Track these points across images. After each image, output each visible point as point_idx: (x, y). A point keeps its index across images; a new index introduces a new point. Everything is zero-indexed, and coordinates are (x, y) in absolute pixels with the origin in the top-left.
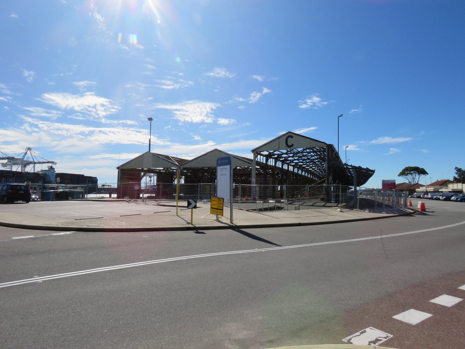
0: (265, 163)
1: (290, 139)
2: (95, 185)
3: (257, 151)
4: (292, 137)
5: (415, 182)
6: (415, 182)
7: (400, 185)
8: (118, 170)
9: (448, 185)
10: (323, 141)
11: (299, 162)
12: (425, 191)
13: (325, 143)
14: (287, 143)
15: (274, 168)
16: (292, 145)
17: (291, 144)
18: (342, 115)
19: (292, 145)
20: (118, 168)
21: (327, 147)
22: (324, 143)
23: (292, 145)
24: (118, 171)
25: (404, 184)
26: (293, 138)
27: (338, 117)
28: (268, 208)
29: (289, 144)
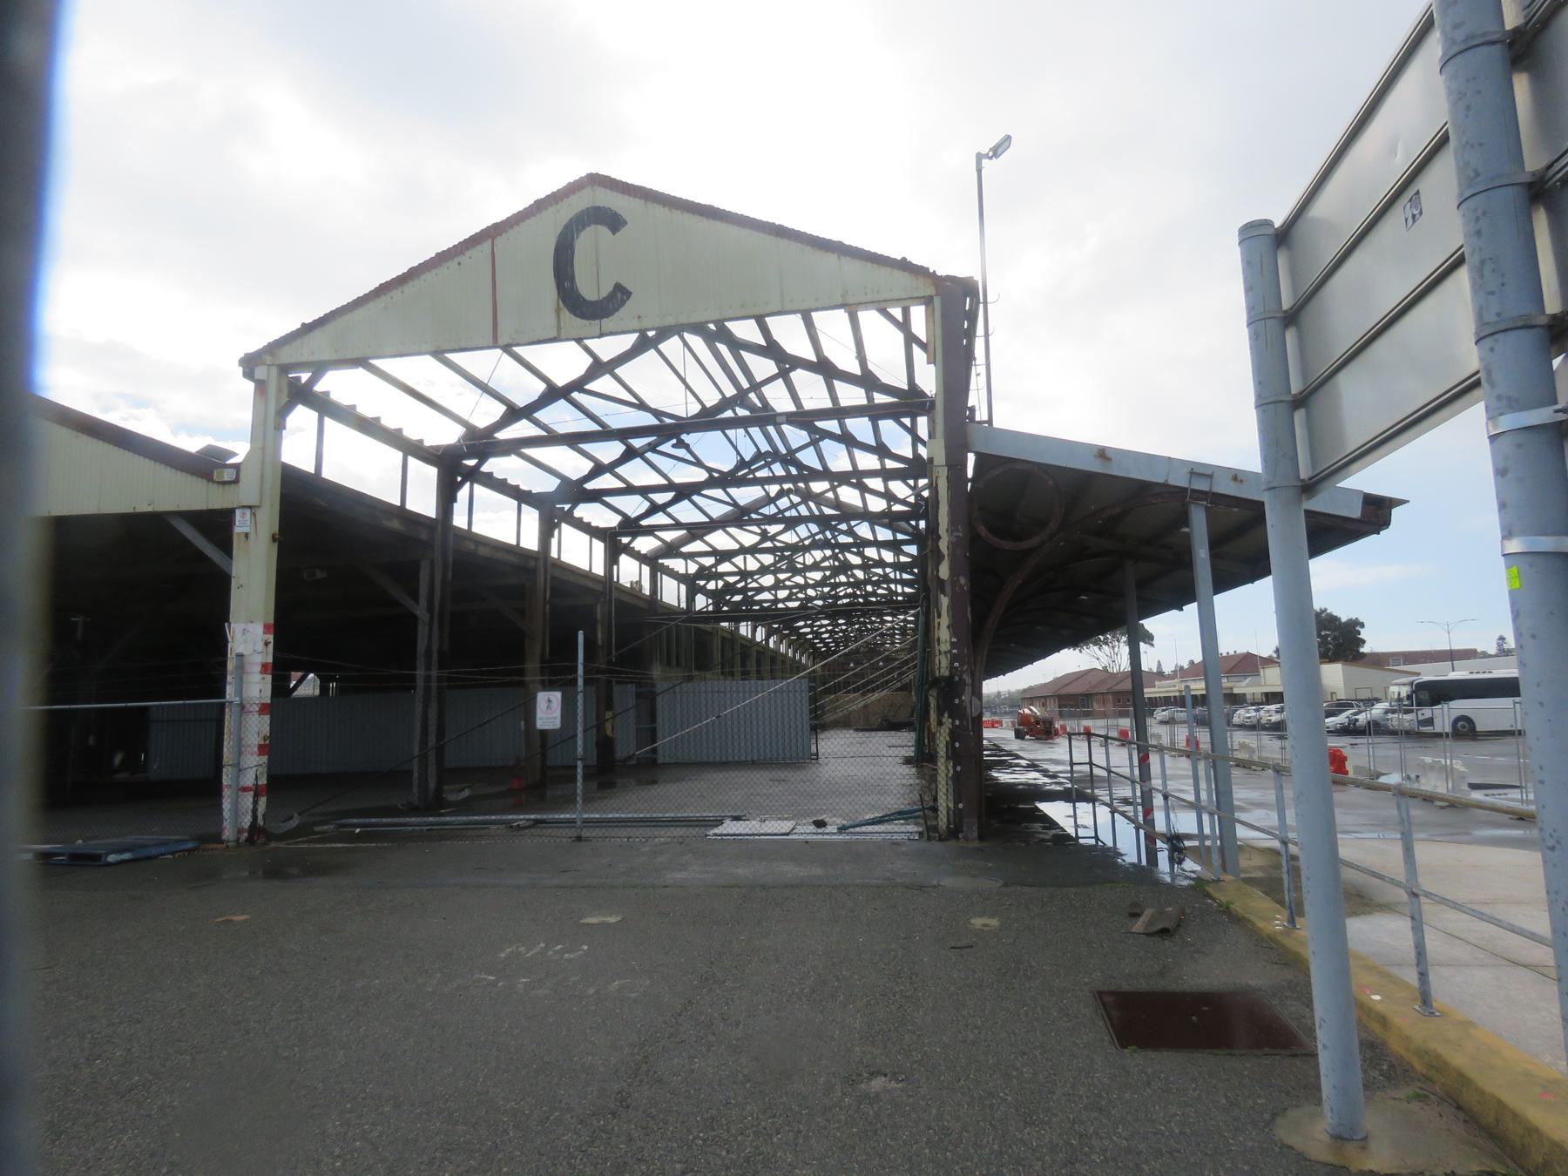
0: (602, 574)
2: (441, 673)
3: (287, 356)
4: (614, 222)
5: (1120, 666)
6: (1120, 666)
7: (1085, 674)
9: (1262, 670)
10: (897, 255)
11: (786, 603)
12: (1175, 697)
13: (920, 272)
14: (572, 279)
15: (776, 652)
16: (612, 295)
17: (606, 290)
21: (937, 301)
22: (904, 265)
25: (1091, 674)
26: (623, 231)
27: (980, 157)
28: (1187, 489)
29: (589, 288)
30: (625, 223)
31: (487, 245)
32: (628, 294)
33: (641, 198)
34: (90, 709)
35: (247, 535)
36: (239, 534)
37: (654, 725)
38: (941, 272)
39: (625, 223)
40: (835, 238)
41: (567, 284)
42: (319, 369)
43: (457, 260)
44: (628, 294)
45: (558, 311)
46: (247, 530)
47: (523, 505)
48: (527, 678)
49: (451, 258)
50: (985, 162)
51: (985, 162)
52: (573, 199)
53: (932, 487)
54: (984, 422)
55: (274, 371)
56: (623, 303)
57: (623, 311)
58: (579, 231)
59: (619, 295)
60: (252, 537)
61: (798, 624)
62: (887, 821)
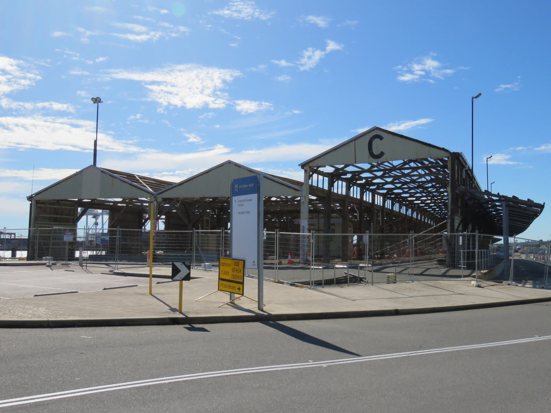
1: (376, 142)
4: (381, 138)
8: (30, 202)
13: (447, 151)
14: (372, 150)
16: (380, 154)
18: (480, 94)
19: (382, 154)
20: (30, 198)
21: (450, 157)
22: (443, 149)
23: (382, 154)
24: (31, 205)
26: (383, 140)
27: (473, 98)
29: (376, 152)
30: (383, 138)
31: (353, 142)
32: (384, 154)
33: (387, 133)
34: (442, 224)
35: (304, 202)
36: (302, 202)
37: (323, 282)
38: (451, 152)
39: (383, 138)
40: (429, 143)
41: (371, 151)
42: (318, 167)
43: (347, 145)
44: (384, 154)
45: (369, 157)
46: (303, 201)
47: (319, 175)
48: (216, 256)
49: (346, 145)
50: (474, 99)
51: (474, 99)
52: (372, 132)
53: (448, 197)
54: (471, 170)
55: (308, 168)
56: (383, 155)
57: (383, 157)
58: (373, 140)
59: (382, 154)
60: (305, 202)
61: (427, 186)
62: (437, 268)
